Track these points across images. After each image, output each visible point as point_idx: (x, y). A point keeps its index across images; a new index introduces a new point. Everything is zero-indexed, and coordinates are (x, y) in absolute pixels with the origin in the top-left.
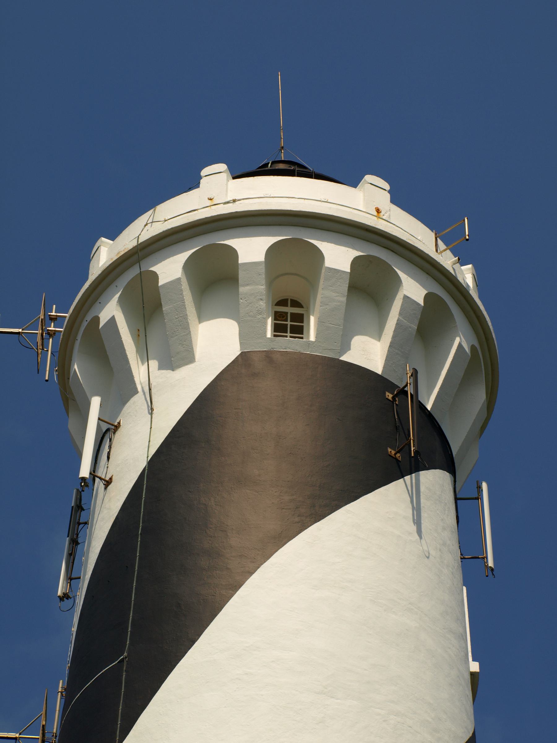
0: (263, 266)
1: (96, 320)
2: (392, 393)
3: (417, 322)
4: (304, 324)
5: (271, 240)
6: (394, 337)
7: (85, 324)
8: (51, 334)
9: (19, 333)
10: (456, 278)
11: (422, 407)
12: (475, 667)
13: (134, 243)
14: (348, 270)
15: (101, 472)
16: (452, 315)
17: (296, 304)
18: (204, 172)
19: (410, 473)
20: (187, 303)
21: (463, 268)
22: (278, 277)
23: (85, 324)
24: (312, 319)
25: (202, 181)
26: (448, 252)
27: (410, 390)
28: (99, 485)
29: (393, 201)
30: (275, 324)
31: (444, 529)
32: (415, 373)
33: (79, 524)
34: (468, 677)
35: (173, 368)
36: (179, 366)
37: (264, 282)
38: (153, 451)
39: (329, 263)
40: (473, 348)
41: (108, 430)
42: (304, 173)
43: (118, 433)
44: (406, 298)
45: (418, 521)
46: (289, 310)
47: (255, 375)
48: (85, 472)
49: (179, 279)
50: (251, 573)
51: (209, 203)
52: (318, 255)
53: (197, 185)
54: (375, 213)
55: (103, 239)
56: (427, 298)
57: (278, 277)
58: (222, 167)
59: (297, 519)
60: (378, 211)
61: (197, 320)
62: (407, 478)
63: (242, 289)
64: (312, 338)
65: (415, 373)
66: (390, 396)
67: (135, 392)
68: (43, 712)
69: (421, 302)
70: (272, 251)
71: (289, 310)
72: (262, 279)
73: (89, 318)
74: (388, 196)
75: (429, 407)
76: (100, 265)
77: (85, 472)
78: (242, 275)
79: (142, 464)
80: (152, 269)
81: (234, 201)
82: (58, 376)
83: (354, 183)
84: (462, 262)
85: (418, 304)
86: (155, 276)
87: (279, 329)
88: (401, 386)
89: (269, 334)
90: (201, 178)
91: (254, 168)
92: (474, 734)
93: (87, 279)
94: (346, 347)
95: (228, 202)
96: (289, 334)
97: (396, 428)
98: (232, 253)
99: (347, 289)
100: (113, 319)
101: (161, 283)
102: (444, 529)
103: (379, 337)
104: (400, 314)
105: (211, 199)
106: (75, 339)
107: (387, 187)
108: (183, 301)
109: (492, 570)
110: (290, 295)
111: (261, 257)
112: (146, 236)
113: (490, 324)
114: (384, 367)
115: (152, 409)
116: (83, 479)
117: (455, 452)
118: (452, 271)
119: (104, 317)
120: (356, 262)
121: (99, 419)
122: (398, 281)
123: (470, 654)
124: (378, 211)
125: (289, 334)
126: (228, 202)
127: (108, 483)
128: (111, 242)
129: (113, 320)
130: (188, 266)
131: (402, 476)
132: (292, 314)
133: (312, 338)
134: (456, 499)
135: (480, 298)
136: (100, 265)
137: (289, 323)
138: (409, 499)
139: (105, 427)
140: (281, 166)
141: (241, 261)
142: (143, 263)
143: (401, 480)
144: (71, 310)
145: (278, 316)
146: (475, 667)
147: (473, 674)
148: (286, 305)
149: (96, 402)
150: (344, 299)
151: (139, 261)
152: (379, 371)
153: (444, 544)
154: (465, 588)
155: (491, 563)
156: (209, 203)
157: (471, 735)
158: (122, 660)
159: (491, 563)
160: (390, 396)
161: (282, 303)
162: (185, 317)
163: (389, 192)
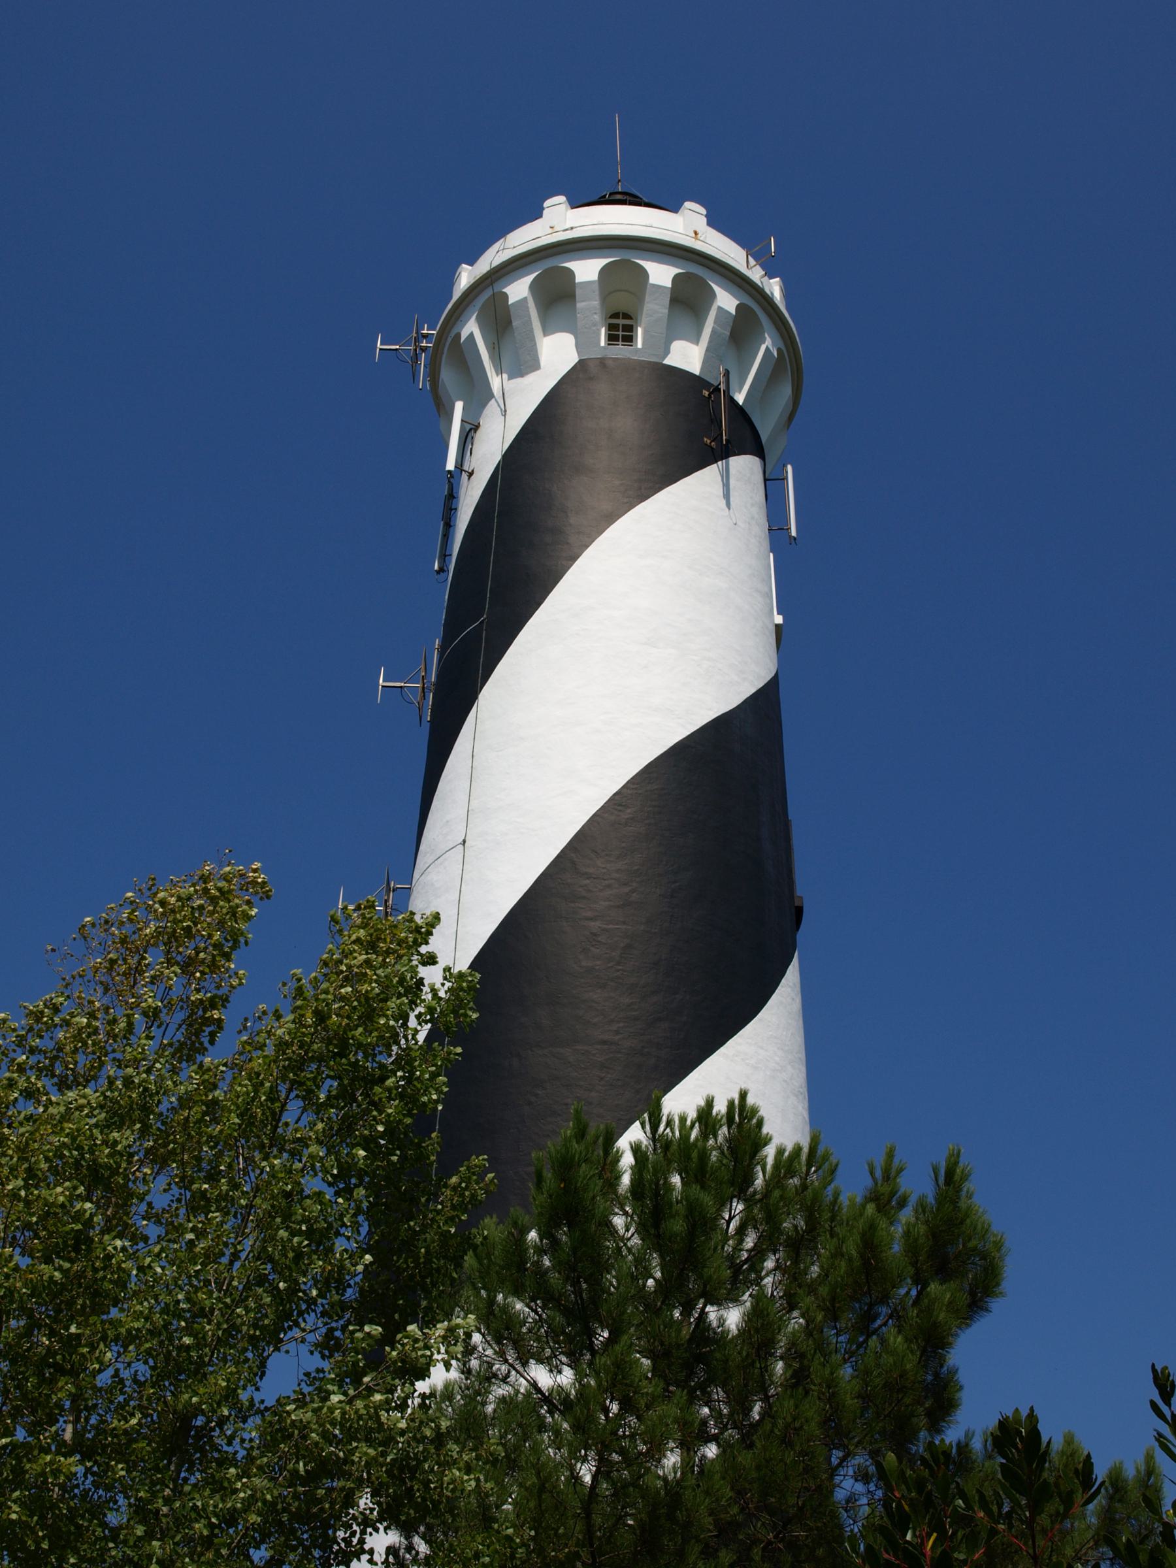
0: (597, 284)
1: (458, 335)
2: (708, 390)
3: (729, 329)
4: (634, 334)
5: (603, 262)
6: (710, 342)
7: (450, 340)
8: (424, 349)
9: (396, 350)
10: (763, 290)
11: (732, 401)
12: (779, 619)
13: (489, 269)
14: (669, 285)
15: (466, 468)
16: (761, 324)
17: (627, 316)
18: (546, 204)
19: (722, 460)
20: (533, 319)
21: (771, 281)
22: (610, 293)
23: (450, 340)
24: (640, 331)
25: (545, 212)
26: (758, 267)
27: (722, 387)
28: (464, 476)
29: (709, 224)
30: (609, 335)
31: (752, 505)
32: (727, 374)
33: (451, 510)
34: (773, 629)
35: (522, 375)
36: (527, 373)
37: (597, 298)
38: (506, 446)
39: (653, 280)
40: (779, 350)
41: (471, 430)
42: (635, 201)
43: (478, 432)
44: (720, 308)
45: (727, 496)
46: (621, 322)
47: (591, 379)
48: (450, 465)
49: (526, 298)
50: (587, 547)
51: (550, 231)
52: (644, 274)
53: (540, 216)
54: (693, 235)
55: (464, 265)
56: (738, 308)
57: (610, 293)
58: (561, 199)
59: (625, 500)
60: (696, 233)
61: (542, 334)
62: (720, 463)
63: (579, 305)
64: (640, 345)
65: (727, 374)
66: (706, 393)
67: (490, 395)
68: (422, 666)
69: (733, 312)
70: (604, 271)
71: (621, 322)
72: (596, 294)
73: (453, 334)
74: (705, 220)
75: (740, 398)
76: (462, 286)
77: (450, 465)
78: (578, 292)
79: (499, 457)
80: (504, 290)
81: (572, 228)
82: (430, 385)
83: (674, 208)
84: (770, 274)
85: (730, 314)
86: (506, 296)
87: (612, 339)
88: (716, 384)
89: (603, 343)
90: (543, 209)
91: (595, 198)
92: (776, 675)
93: (451, 298)
94: (667, 352)
95: (567, 230)
96: (620, 343)
97: (712, 421)
98: (570, 274)
99: (668, 302)
100: (471, 335)
101: (511, 302)
102: (752, 505)
103: (696, 341)
104: (715, 322)
105: (552, 228)
106: (443, 353)
107: (704, 211)
108: (529, 317)
109: (795, 539)
110: (623, 308)
111: (668, 284)
112: (496, 263)
113: (794, 329)
114: (702, 369)
115: (505, 411)
116: (449, 472)
117: (764, 441)
118: (760, 284)
119: (464, 334)
120: (676, 278)
121: (462, 421)
122: (713, 296)
123: (775, 609)
124: (696, 233)
125: (620, 343)
126: (567, 230)
127: (471, 474)
128: (470, 268)
129: (471, 335)
130: (533, 287)
131: (716, 462)
132: (623, 325)
133: (640, 345)
134: (765, 480)
135: (787, 309)
136: (462, 286)
137: (621, 333)
138: (720, 478)
139: (468, 427)
140: (619, 197)
141: (577, 280)
142: (495, 285)
143: (715, 465)
144: (438, 328)
145: (611, 327)
146: (779, 619)
147: (777, 626)
148: (618, 318)
149: (459, 406)
150: (667, 311)
151: (492, 284)
152: (697, 372)
153: (753, 518)
154: (771, 555)
155: (794, 533)
156: (550, 231)
157: (773, 674)
158: (483, 621)
159: (794, 533)
160: (706, 393)
161: (615, 315)
162: (531, 331)
163: (706, 216)
